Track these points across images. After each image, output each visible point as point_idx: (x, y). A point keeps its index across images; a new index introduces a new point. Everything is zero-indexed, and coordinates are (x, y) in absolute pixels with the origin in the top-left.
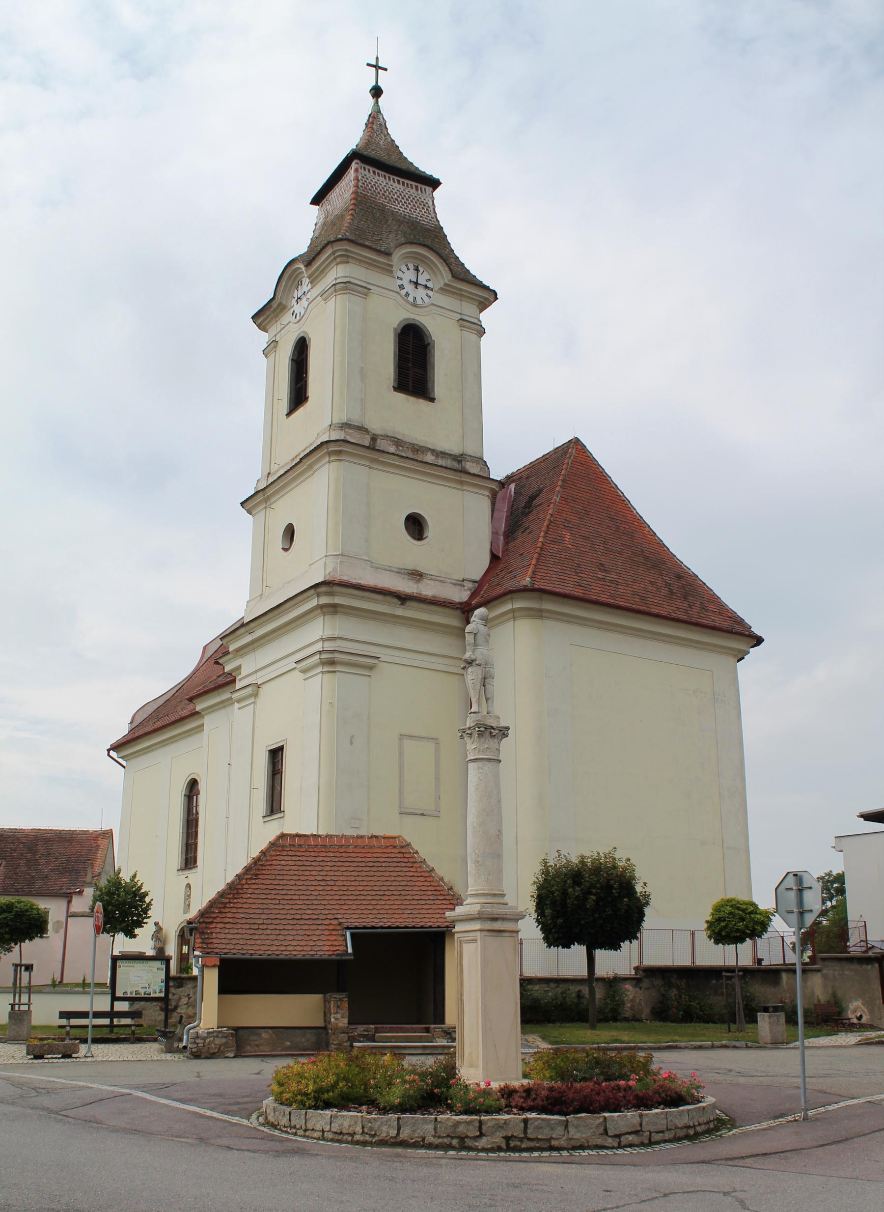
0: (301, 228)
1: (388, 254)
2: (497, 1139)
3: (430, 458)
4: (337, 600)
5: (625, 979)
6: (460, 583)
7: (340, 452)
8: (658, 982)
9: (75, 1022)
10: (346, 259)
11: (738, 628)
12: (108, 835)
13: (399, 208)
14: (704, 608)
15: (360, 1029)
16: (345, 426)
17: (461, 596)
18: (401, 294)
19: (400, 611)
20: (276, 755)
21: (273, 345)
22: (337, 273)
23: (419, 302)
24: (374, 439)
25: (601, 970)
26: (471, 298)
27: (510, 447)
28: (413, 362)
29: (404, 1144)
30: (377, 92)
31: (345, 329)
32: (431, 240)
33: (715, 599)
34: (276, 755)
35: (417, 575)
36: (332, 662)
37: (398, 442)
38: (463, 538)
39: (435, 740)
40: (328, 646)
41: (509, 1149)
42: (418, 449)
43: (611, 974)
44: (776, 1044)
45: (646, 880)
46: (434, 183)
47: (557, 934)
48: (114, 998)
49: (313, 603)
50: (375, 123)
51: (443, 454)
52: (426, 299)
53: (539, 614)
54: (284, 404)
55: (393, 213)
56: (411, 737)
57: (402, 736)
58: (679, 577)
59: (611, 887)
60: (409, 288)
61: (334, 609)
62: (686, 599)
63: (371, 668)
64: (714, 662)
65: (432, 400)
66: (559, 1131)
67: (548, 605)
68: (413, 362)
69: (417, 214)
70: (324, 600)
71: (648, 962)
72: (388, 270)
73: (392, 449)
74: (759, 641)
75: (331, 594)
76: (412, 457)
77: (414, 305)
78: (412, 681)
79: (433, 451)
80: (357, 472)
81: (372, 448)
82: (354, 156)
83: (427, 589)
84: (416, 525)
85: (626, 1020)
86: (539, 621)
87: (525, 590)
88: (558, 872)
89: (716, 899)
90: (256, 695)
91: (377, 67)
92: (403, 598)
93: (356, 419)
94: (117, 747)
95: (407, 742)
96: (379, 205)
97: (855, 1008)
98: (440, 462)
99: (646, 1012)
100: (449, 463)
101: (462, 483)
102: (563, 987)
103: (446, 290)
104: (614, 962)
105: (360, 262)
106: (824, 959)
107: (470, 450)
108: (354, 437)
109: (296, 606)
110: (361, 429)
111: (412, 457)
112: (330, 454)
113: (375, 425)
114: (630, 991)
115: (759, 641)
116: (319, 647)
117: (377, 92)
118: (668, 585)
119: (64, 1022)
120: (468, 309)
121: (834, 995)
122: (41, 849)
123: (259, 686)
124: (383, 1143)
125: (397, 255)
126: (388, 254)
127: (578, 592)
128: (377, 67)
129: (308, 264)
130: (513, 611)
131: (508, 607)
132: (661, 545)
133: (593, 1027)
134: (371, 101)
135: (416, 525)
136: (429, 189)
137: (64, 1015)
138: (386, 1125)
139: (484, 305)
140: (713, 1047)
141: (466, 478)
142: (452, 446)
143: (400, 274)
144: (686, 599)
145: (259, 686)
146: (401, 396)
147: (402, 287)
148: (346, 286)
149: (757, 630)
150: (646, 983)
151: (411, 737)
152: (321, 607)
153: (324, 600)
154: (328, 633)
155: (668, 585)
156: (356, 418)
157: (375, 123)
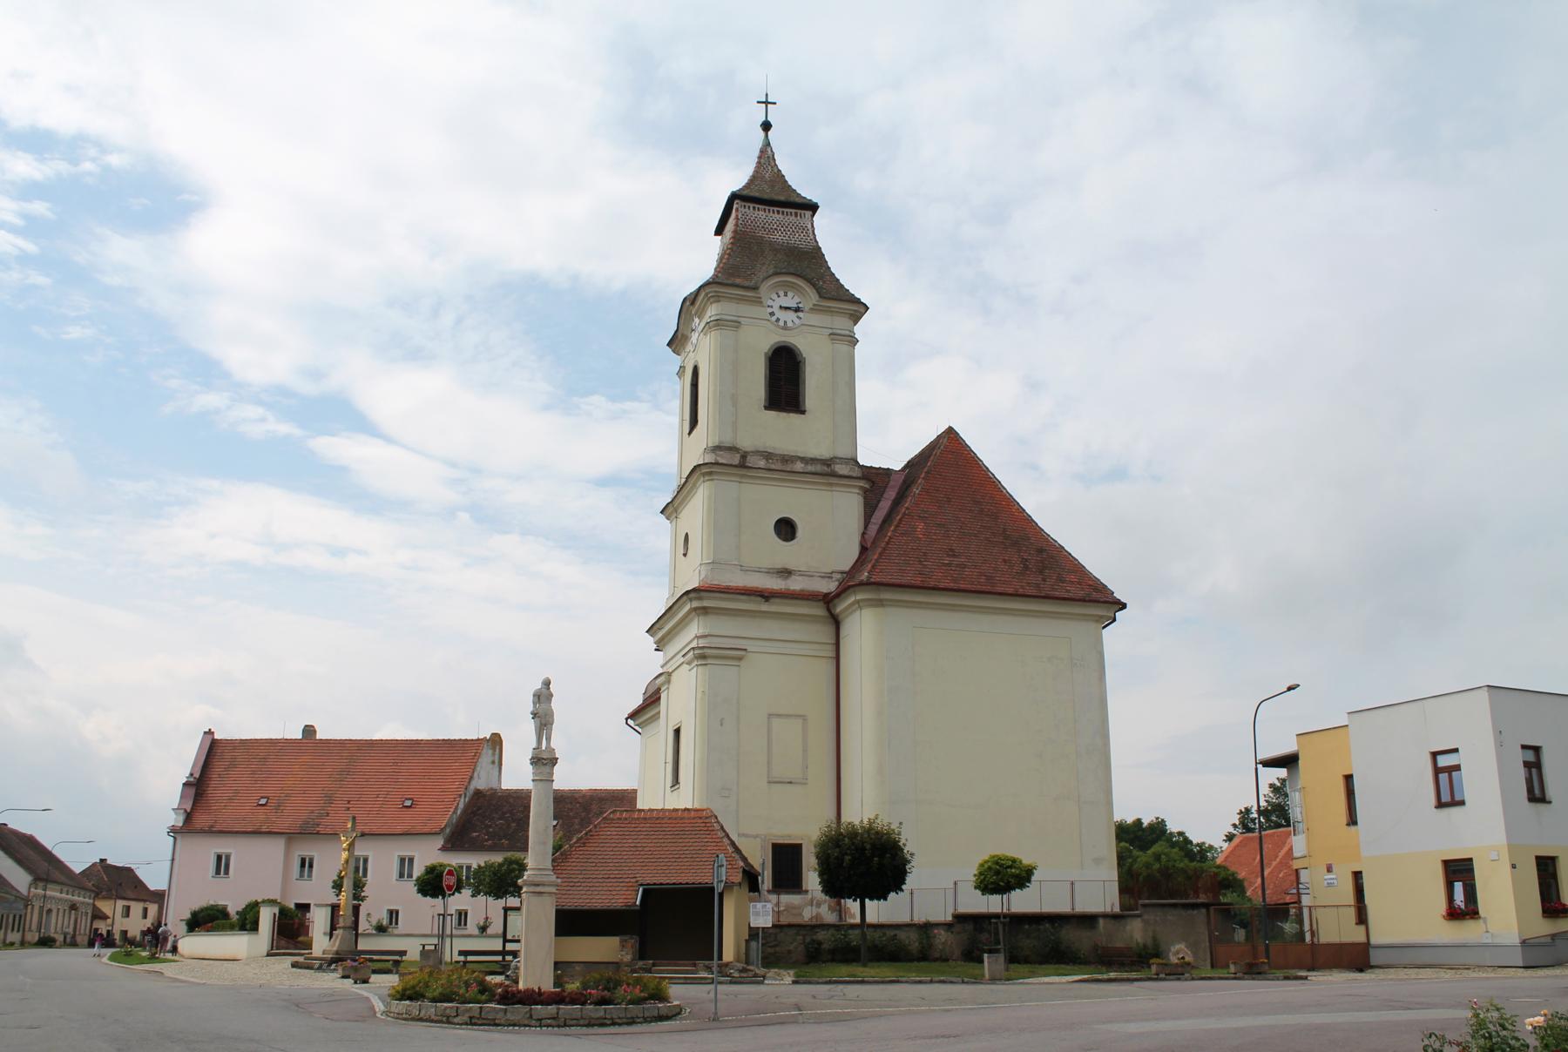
0: (702, 257)
1: (755, 288)
2: (465, 1018)
3: (799, 466)
4: (706, 603)
5: (937, 925)
6: (829, 576)
7: (710, 473)
8: (970, 927)
9: (470, 958)
10: (717, 298)
11: (1095, 595)
12: (635, 791)
13: (778, 237)
14: (1061, 579)
15: (640, 964)
16: (717, 448)
17: (829, 587)
18: (779, 315)
19: (765, 607)
20: (677, 732)
21: (682, 368)
22: (712, 311)
23: (790, 324)
24: (744, 456)
25: (871, 918)
26: (840, 313)
27: (888, 443)
28: (785, 380)
29: (421, 1020)
30: (766, 126)
31: (733, 356)
32: (808, 266)
33: (1078, 569)
34: (677, 732)
35: (786, 573)
36: (703, 657)
37: (768, 456)
38: (833, 530)
39: (803, 718)
40: (702, 643)
41: (472, 1024)
42: (787, 459)
43: (923, 920)
44: (994, 980)
45: (910, 842)
46: (813, 208)
47: (835, 886)
48: (505, 941)
49: (687, 608)
50: (766, 156)
51: (813, 461)
52: (797, 321)
53: (880, 603)
54: (687, 429)
55: (771, 243)
56: (779, 716)
57: (770, 716)
58: (1040, 551)
59: (864, 849)
60: (779, 314)
61: (704, 611)
62: (1041, 572)
63: (740, 659)
64: (1086, 628)
65: (803, 412)
66: (500, 1015)
67: (887, 595)
68: (785, 380)
69: (796, 240)
70: (695, 604)
71: (962, 910)
72: (758, 302)
73: (762, 463)
74: (1124, 606)
75: (700, 599)
76: (781, 466)
77: (785, 328)
78: (781, 662)
79: (803, 460)
80: (731, 488)
81: (742, 465)
82: (734, 197)
83: (796, 584)
84: (786, 529)
85: (936, 960)
86: (879, 610)
87: (861, 584)
88: (853, 834)
89: (984, 856)
90: (669, 682)
91: (767, 103)
92: (766, 595)
93: (728, 441)
94: (632, 716)
95: (776, 722)
96: (769, 236)
97: (1178, 951)
98: (810, 468)
99: (957, 952)
100: (819, 468)
101: (831, 484)
102: (890, 933)
103: (815, 309)
104: (877, 911)
105: (731, 299)
106: (1144, 906)
107: (842, 452)
108: (724, 458)
109: (681, 608)
110: (732, 449)
111: (781, 466)
112: (704, 474)
113: (746, 443)
114: (942, 936)
115: (1124, 606)
116: (694, 644)
117: (766, 126)
118: (1024, 561)
119: (462, 958)
120: (840, 323)
121: (1155, 939)
122: (594, 807)
123: (669, 674)
124: (413, 1019)
125: (764, 288)
126: (755, 288)
127: (918, 581)
128: (767, 103)
129: (693, 303)
130: (858, 602)
131: (852, 599)
132: (1029, 520)
133: (865, 965)
134: (762, 134)
135: (786, 529)
136: (808, 213)
137: (461, 953)
138: (430, 1009)
139: (856, 318)
140: (931, 982)
141: (834, 480)
142: (823, 451)
143: (770, 303)
144: (1041, 572)
145: (669, 674)
146: (773, 413)
147: (772, 314)
148: (718, 323)
149: (1119, 595)
150: (958, 928)
151: (779, 716)
152: (695, 609)
153: (695, 604)
154: (701, 632)
155: (1024, 561)
156: (728, 441)
157: (766, 156)
